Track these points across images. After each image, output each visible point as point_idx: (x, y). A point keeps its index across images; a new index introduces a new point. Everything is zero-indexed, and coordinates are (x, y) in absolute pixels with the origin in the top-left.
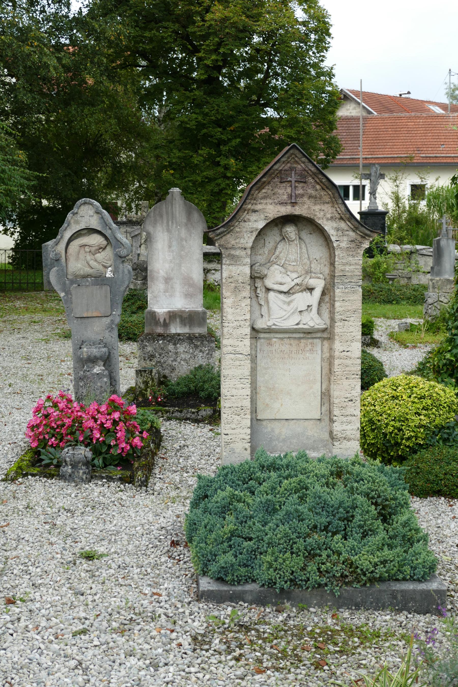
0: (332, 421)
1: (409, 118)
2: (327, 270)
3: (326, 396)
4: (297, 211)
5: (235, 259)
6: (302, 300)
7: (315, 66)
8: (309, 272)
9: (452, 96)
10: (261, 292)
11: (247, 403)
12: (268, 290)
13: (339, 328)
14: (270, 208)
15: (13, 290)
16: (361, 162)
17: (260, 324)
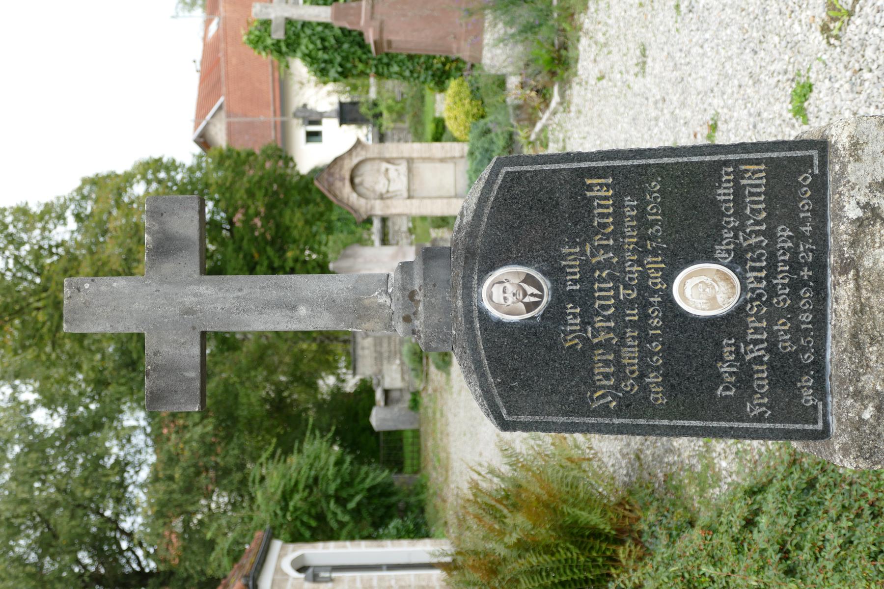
0: (454, 158)
1: (227, 62)
2: (377, 162)
3: (442, 160)
4: (347, 176)
5: (372, 208)
6: (392, 174)
7: (191, 170)
8: (378, 171)
9: (193, 4)
10: (389, 195)
11: (445, 201)
12: (388, 192)
13: (406, 155)
14: (346, 191)
15: (419, 458)
16: (279, 119)
17: (405, 195)
